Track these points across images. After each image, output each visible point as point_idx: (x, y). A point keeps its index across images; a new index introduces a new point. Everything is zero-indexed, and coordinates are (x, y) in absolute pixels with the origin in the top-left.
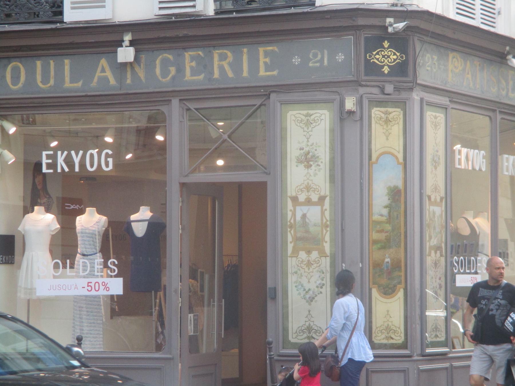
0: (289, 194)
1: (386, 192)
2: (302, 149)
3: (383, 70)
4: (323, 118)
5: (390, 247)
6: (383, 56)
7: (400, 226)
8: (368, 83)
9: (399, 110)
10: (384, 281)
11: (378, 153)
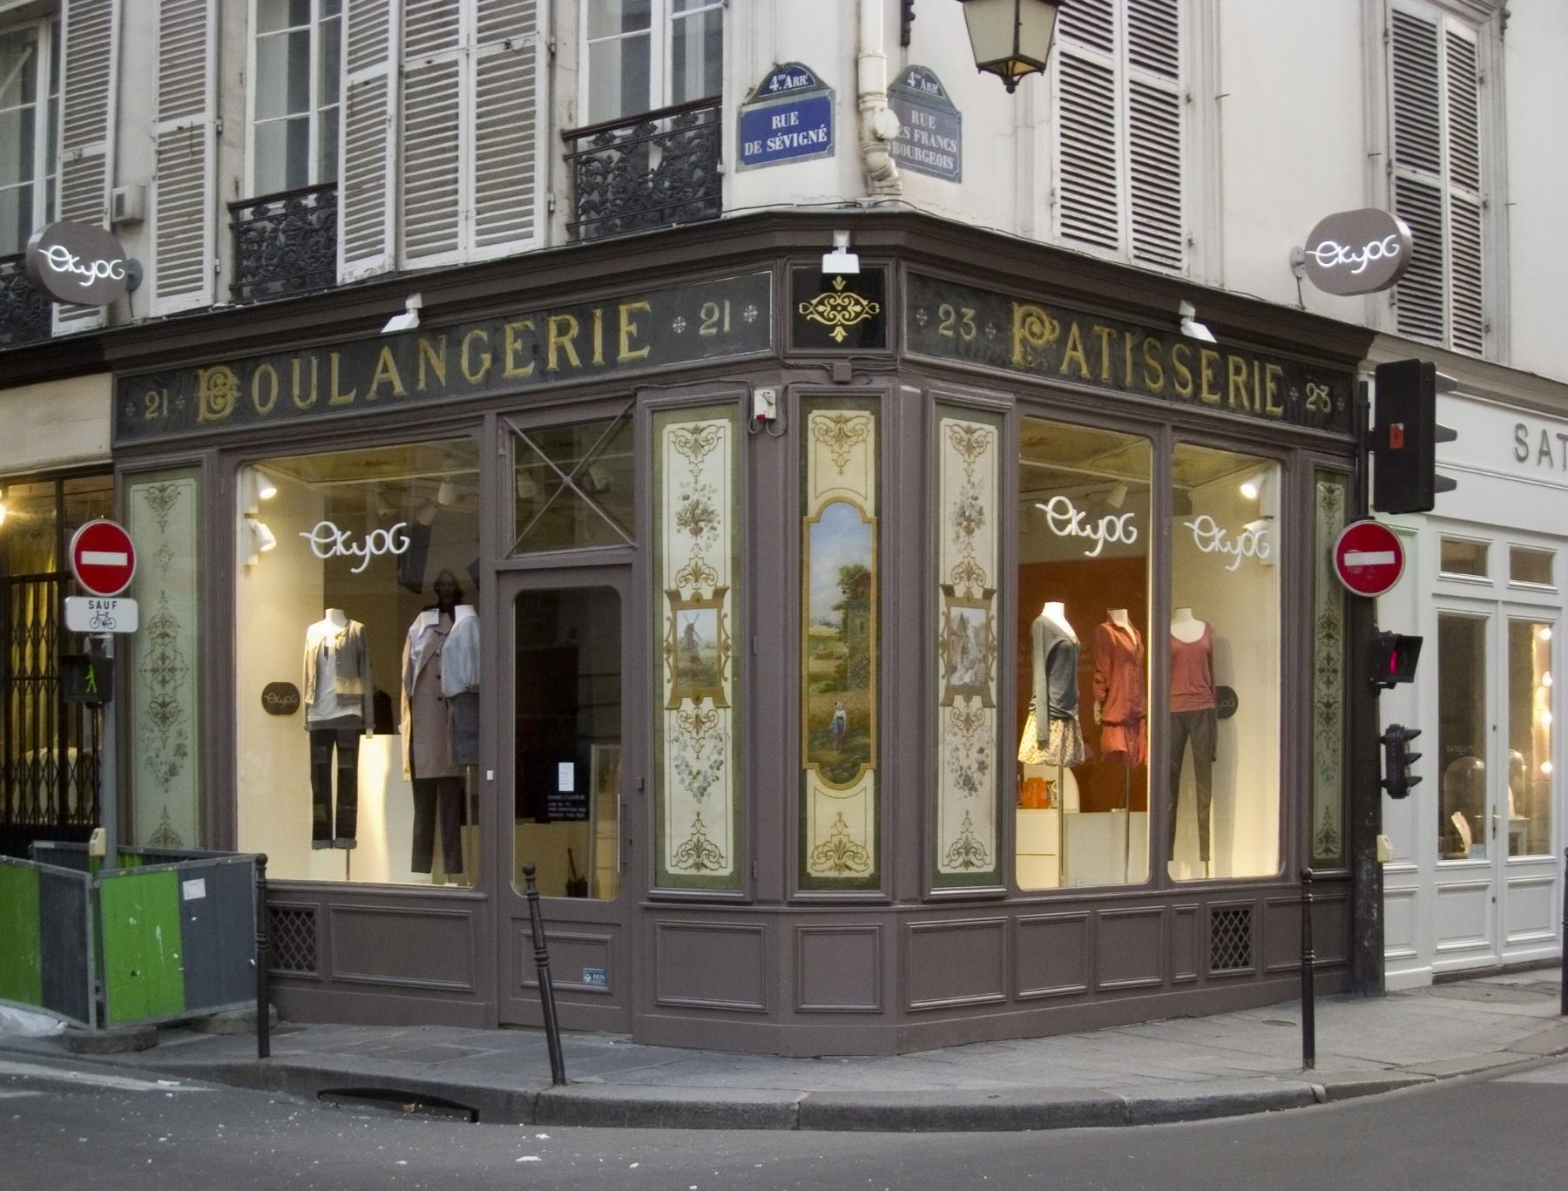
0: (665, 587)
1: (837, 577)
2: (686, 498)
4: (721, 431)
5: (845, 688)
6: (834, 308)
8: (802, 362)
10: (833, 756)
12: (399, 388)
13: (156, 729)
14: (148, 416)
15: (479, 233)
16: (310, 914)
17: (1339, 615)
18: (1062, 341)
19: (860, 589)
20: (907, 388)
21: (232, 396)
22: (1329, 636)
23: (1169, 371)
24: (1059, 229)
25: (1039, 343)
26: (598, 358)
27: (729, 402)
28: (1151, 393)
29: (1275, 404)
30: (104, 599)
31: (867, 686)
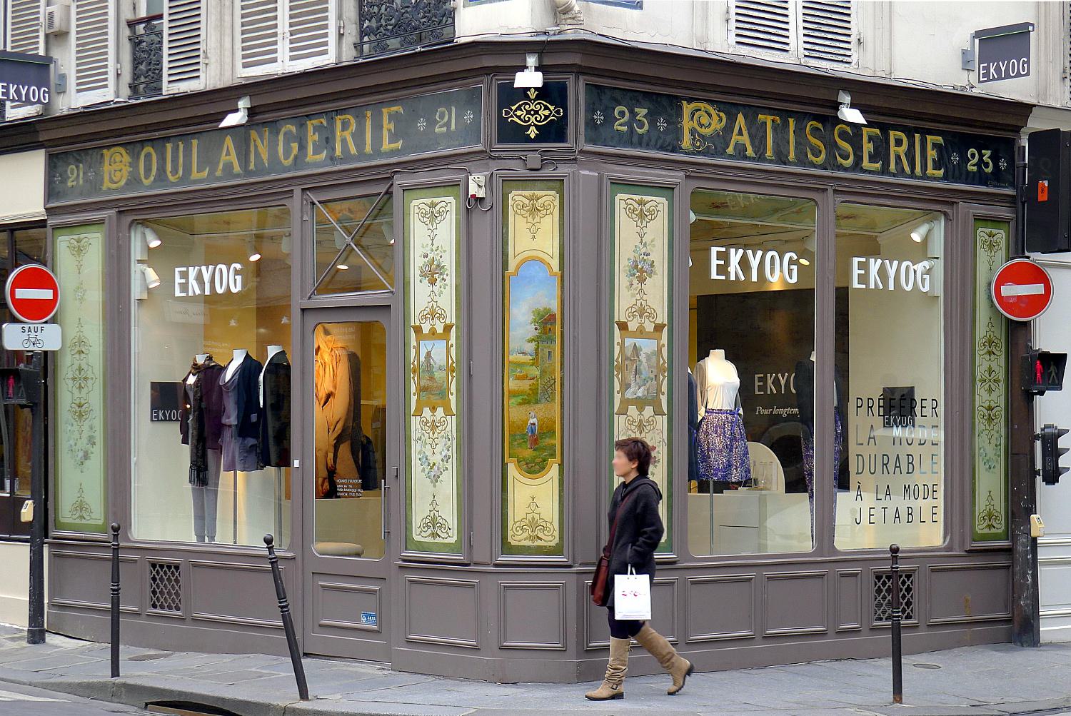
0: (412, 324)
1: (531, 317)
2: (425, 256)
3: (529, 133)
4: (449, 204)
5: (537, 402)
6: (528, 112)
7: (554, 370)
9: (553, 192)
11: (519, 258)
12: (237, 168)
13: (75, 423)
14: (70, 184)
15: (292, 50)
16: (177, 568)
17: (999, 334)
18: (728, 129)
19: (549, 326)
20: (587, 173)
21: (126, 170)
22: (990, 353)
23: (832, 147)
24: (733, 39)
25: (707, 132)
26: (368, 149)
27: (455, 185)
28: (814, 166)
29: (936, 167)
30: (34, 324)
31: (553, 400)
